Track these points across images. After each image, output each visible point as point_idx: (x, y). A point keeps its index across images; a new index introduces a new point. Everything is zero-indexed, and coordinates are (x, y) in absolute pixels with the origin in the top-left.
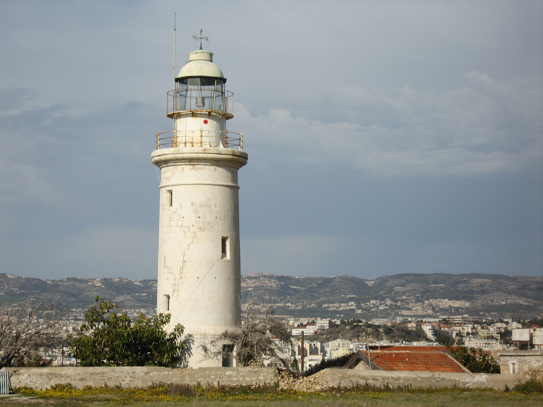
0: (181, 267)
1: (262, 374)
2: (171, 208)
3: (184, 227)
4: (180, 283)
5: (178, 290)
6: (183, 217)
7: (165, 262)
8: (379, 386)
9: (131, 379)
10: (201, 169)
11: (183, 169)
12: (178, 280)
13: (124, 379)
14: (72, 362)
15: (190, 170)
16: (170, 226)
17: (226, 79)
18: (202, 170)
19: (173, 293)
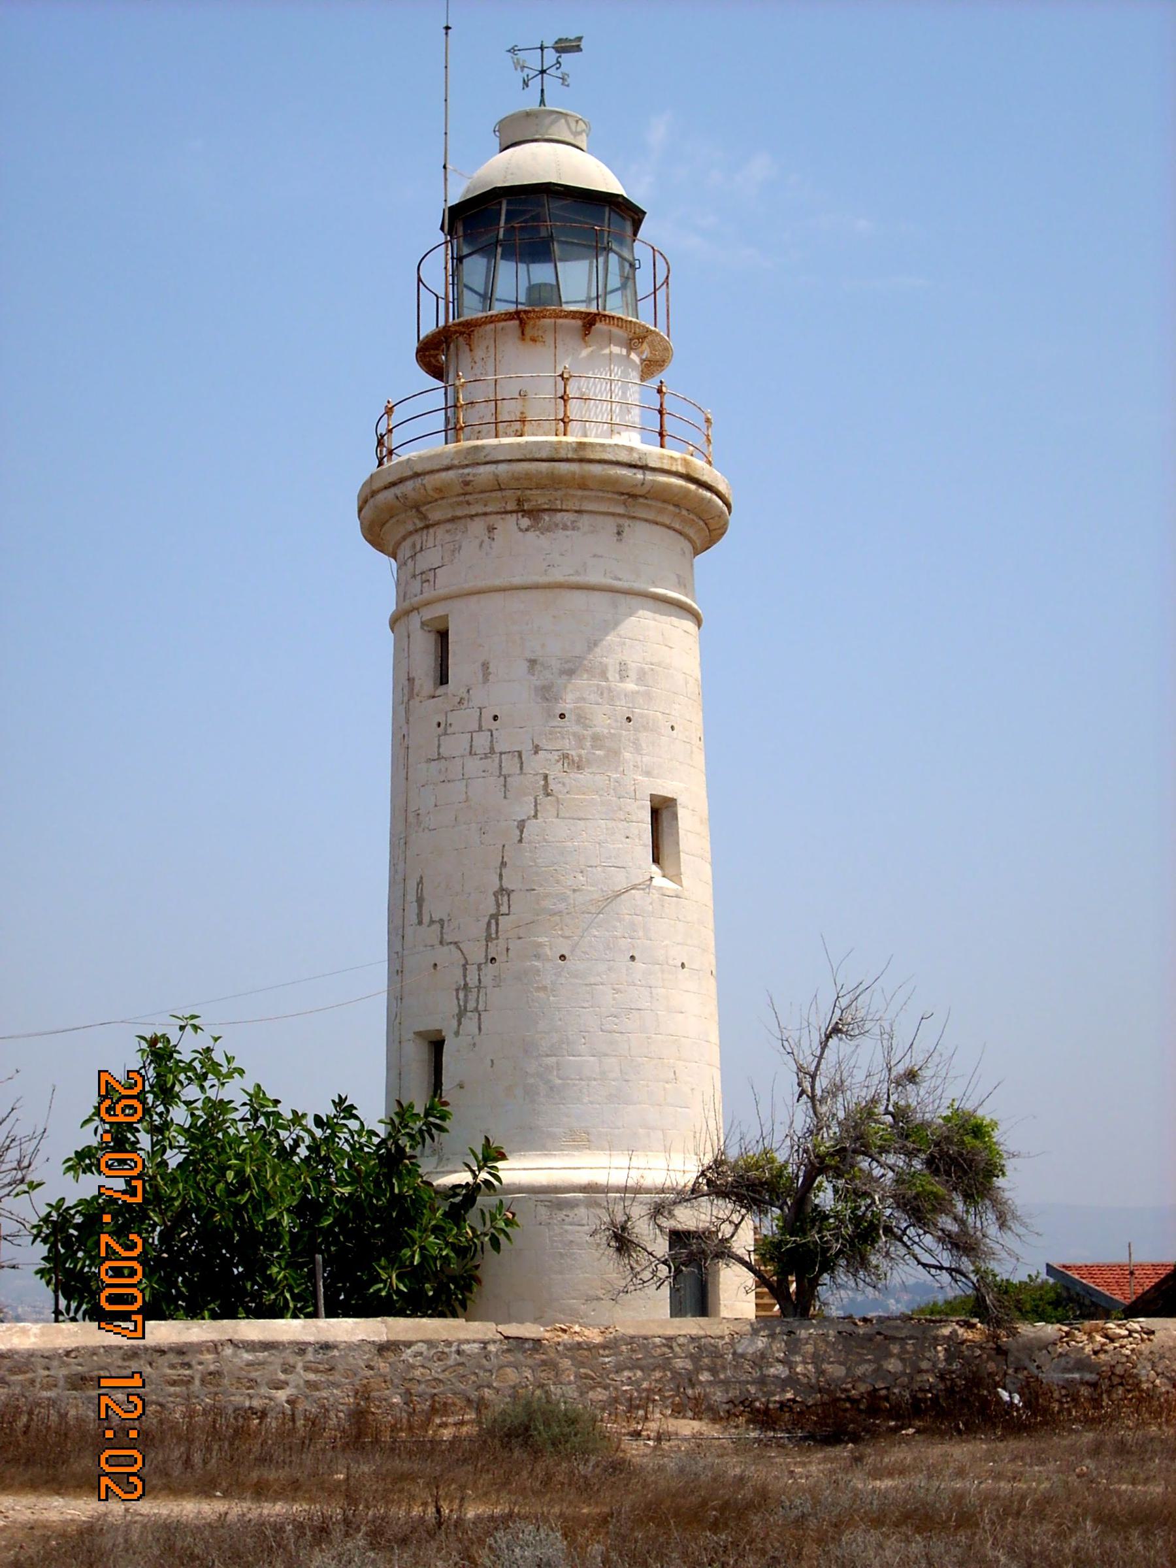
0: (492, 916)
1: (895, 1349)
2: (441, 690)
3: (501, 754)
4: (487, 980)
5: (481, 1007)
6: (495, 718)
7: (420, 901)
8: (386, 1339)
9: (312, 1377)
10: (565, 528)
11: (491, 529)
12: (479, 965)
13: (282, 1377)
14: (668, 1444)
15: (521, 533)
16: (440, 757)
17: (644, 213)
18: (568, 533)
19: (460, 1023)
